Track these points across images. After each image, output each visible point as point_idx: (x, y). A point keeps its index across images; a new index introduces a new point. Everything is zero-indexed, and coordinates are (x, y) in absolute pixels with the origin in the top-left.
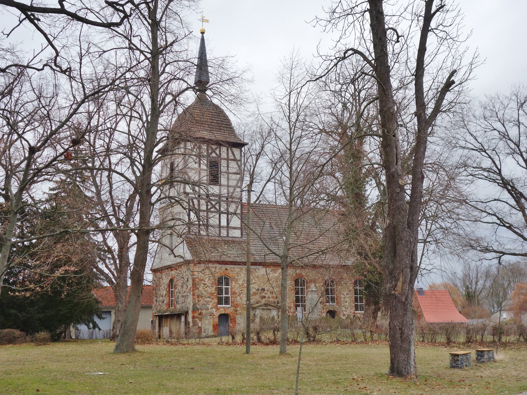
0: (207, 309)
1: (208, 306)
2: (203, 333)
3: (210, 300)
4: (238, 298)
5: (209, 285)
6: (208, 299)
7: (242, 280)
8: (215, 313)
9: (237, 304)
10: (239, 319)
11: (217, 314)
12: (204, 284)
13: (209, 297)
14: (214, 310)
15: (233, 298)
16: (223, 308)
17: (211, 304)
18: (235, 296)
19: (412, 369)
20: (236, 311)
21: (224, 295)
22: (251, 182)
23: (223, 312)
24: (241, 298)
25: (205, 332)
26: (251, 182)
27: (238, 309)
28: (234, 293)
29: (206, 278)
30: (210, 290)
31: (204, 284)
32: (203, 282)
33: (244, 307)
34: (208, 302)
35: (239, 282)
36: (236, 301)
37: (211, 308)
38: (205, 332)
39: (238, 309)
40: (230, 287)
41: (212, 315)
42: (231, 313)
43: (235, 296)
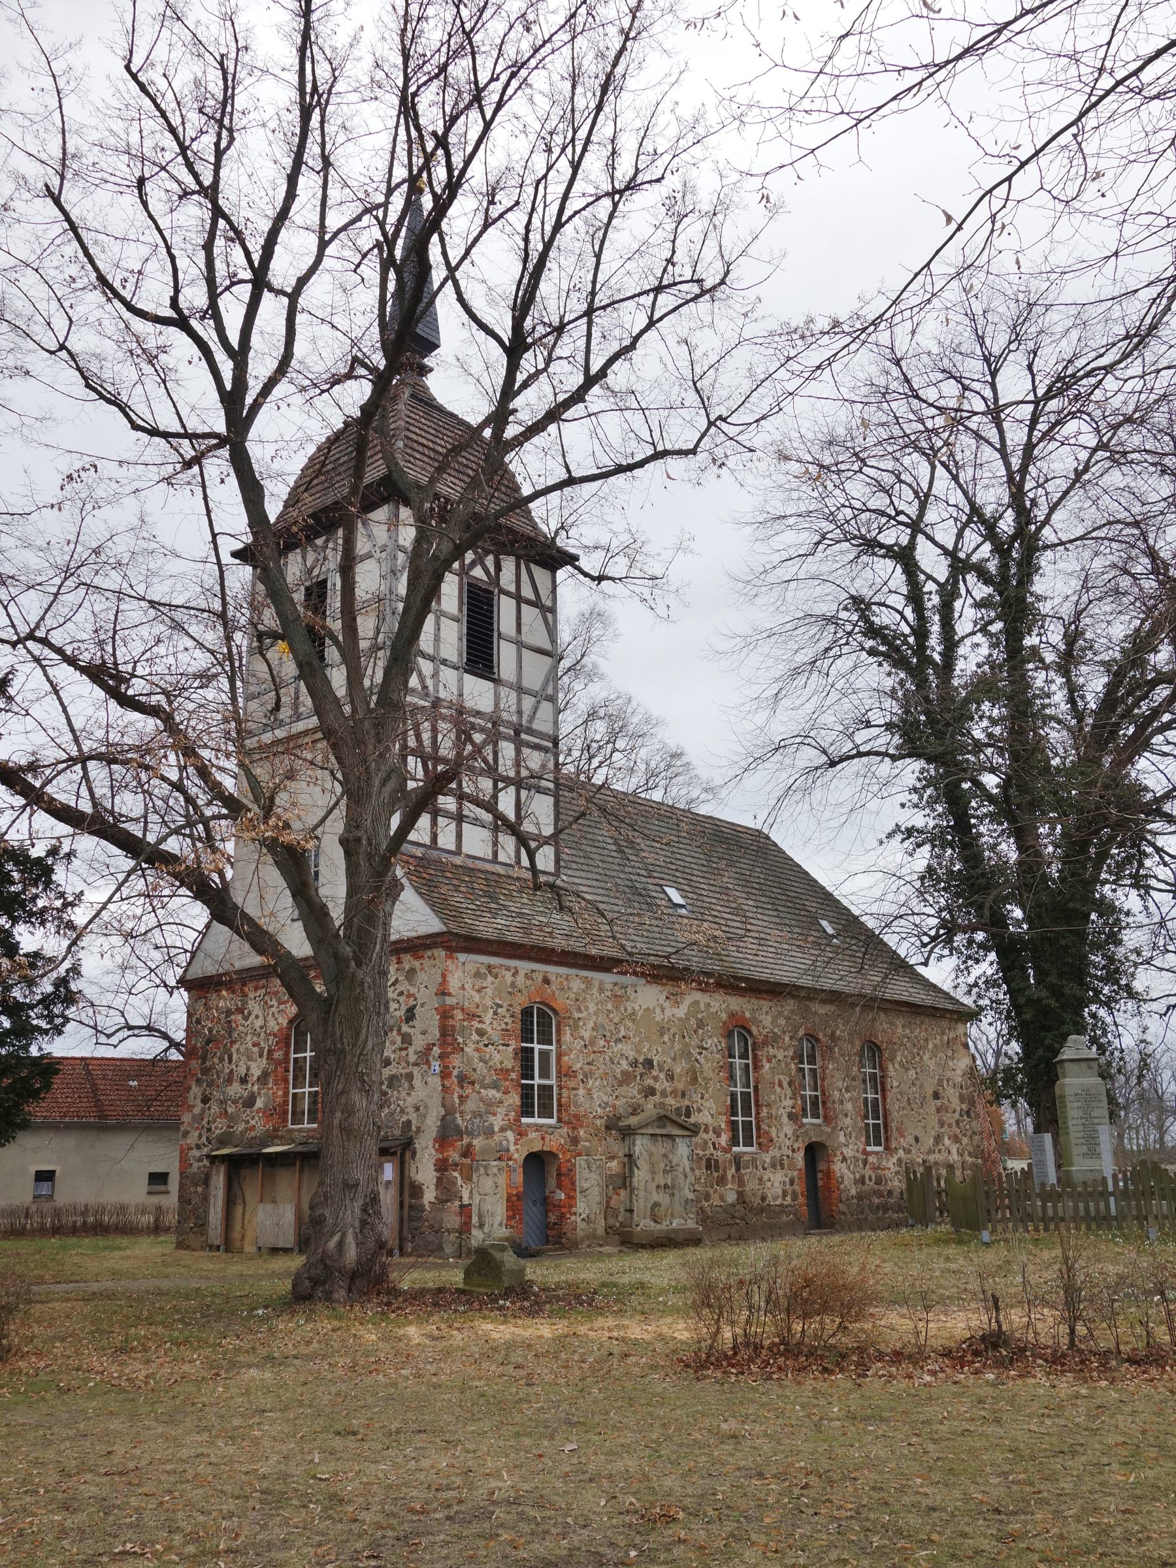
0: (489, 1132)
1: (491, 1118)
3: (498, 1095)
4: (581, 1092)
6: (492, 1093)
8: (512, 1148)
11: (519, 1154)
13: (495, 1085)
20: (575, 1140)
29: (485, 1010)
37: (502, 1130)
41: (503, 1155)
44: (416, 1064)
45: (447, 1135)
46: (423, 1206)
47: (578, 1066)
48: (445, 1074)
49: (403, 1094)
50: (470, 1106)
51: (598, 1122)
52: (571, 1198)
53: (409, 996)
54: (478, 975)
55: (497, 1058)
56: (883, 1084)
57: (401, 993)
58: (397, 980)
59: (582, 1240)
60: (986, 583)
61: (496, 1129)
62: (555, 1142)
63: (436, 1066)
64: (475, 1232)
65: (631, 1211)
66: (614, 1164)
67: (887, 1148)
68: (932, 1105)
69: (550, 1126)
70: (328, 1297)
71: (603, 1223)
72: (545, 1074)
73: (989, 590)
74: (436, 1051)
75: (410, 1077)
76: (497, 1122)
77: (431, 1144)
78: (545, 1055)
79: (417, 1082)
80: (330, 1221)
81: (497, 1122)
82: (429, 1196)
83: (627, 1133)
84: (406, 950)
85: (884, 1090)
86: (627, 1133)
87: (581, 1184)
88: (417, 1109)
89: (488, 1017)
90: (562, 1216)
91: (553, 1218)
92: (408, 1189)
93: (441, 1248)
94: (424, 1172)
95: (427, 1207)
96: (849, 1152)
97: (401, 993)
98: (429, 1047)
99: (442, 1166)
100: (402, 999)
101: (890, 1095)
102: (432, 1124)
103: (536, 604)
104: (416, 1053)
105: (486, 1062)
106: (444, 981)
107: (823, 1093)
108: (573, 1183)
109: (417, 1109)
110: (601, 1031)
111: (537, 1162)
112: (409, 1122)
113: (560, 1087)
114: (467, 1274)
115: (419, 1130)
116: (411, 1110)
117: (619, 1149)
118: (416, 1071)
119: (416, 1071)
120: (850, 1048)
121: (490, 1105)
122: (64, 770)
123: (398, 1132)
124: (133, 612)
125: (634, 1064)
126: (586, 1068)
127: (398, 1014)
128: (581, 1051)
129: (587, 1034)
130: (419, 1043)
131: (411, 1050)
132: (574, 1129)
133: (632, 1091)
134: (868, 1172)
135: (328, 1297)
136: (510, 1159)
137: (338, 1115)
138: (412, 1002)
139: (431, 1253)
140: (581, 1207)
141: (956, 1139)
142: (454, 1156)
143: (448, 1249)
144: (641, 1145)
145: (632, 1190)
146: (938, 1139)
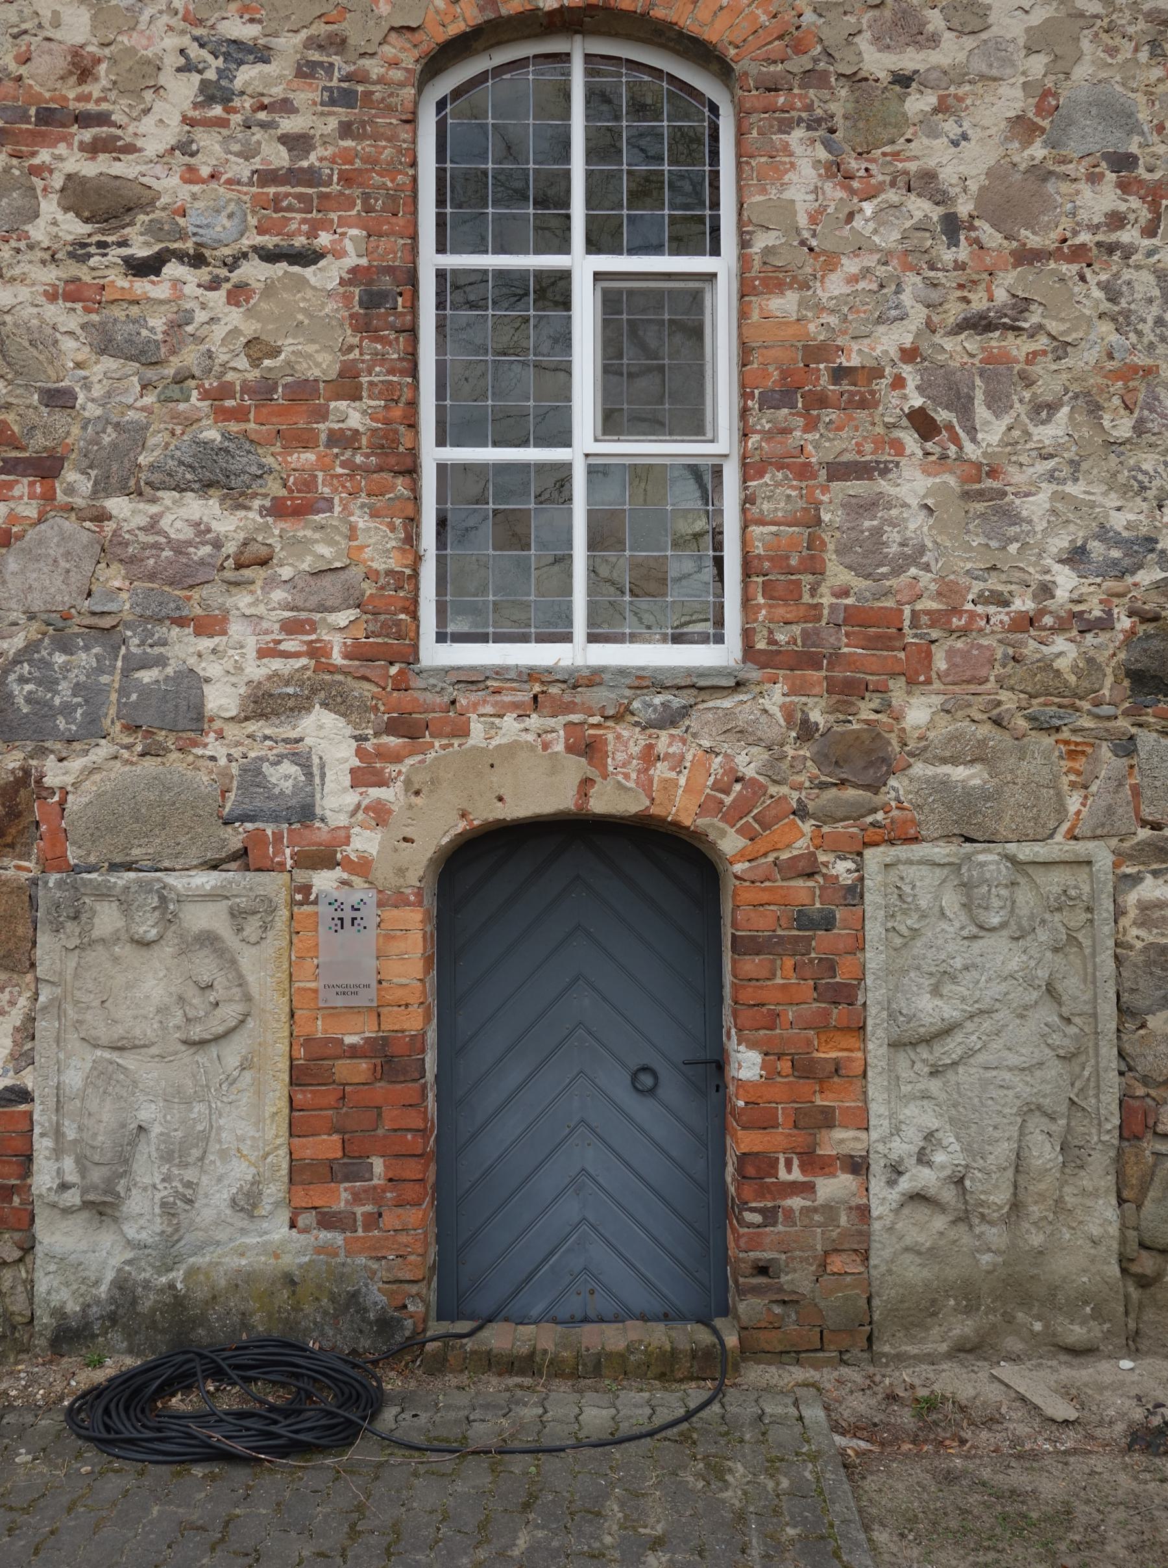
0: (177, 716)
1: (185, 648)
2: (56, 1237)
3: (230, 525)
4: (912, 483)
5: (220, 221)
6: (185, 513)
7: (1011, 99)
8: (337, 800)
9: (876, 626)
10: (945, 939)
11: (389, 830)
12: (106, 207)
13: (213, 476)
14: (328, 735)
15: (780, 495)
16: (542, 692)
17: (255, 610)
18: (820, 446)
19: (13, 831)
20: (864, 759)
21: (586, 440)
22: (1095, 969)
23: (541, 790)
24: (983, 492)
25: (102, 1209)
26: (1095, 969)
27: (918, 712)
28: (801, 384)
29: (143, 79)
30: (222, 324)
31: (106, 207)
32: (68, 159)
33: (1046, 683)
34: (181, 588)
35: (932, 153)
36: (868, 554)
37: (263, 704)
38: (102, 1209)
39: (918, 712)
40: (722, 265)
41: (268, 835)
42: (746, 803)
43: (820, 446)
47: (889, 341)
51: (1064, 651)
59: (921, 1311)
61: (221, 699)
69: (700, 686)
71: (1104, 1217)
76: (226, 669)
87: (895, 986)
89: (157, 130)
105: (144, 355)
108: (845, 994)
110: (1091, 138)
121: (186, 577)
122: (1085, 969)
124: (868, 1328)
126: (959, 350)
128: (913, 256)
129: (966, 158)
132: (846, 692)
136: (325, 859)
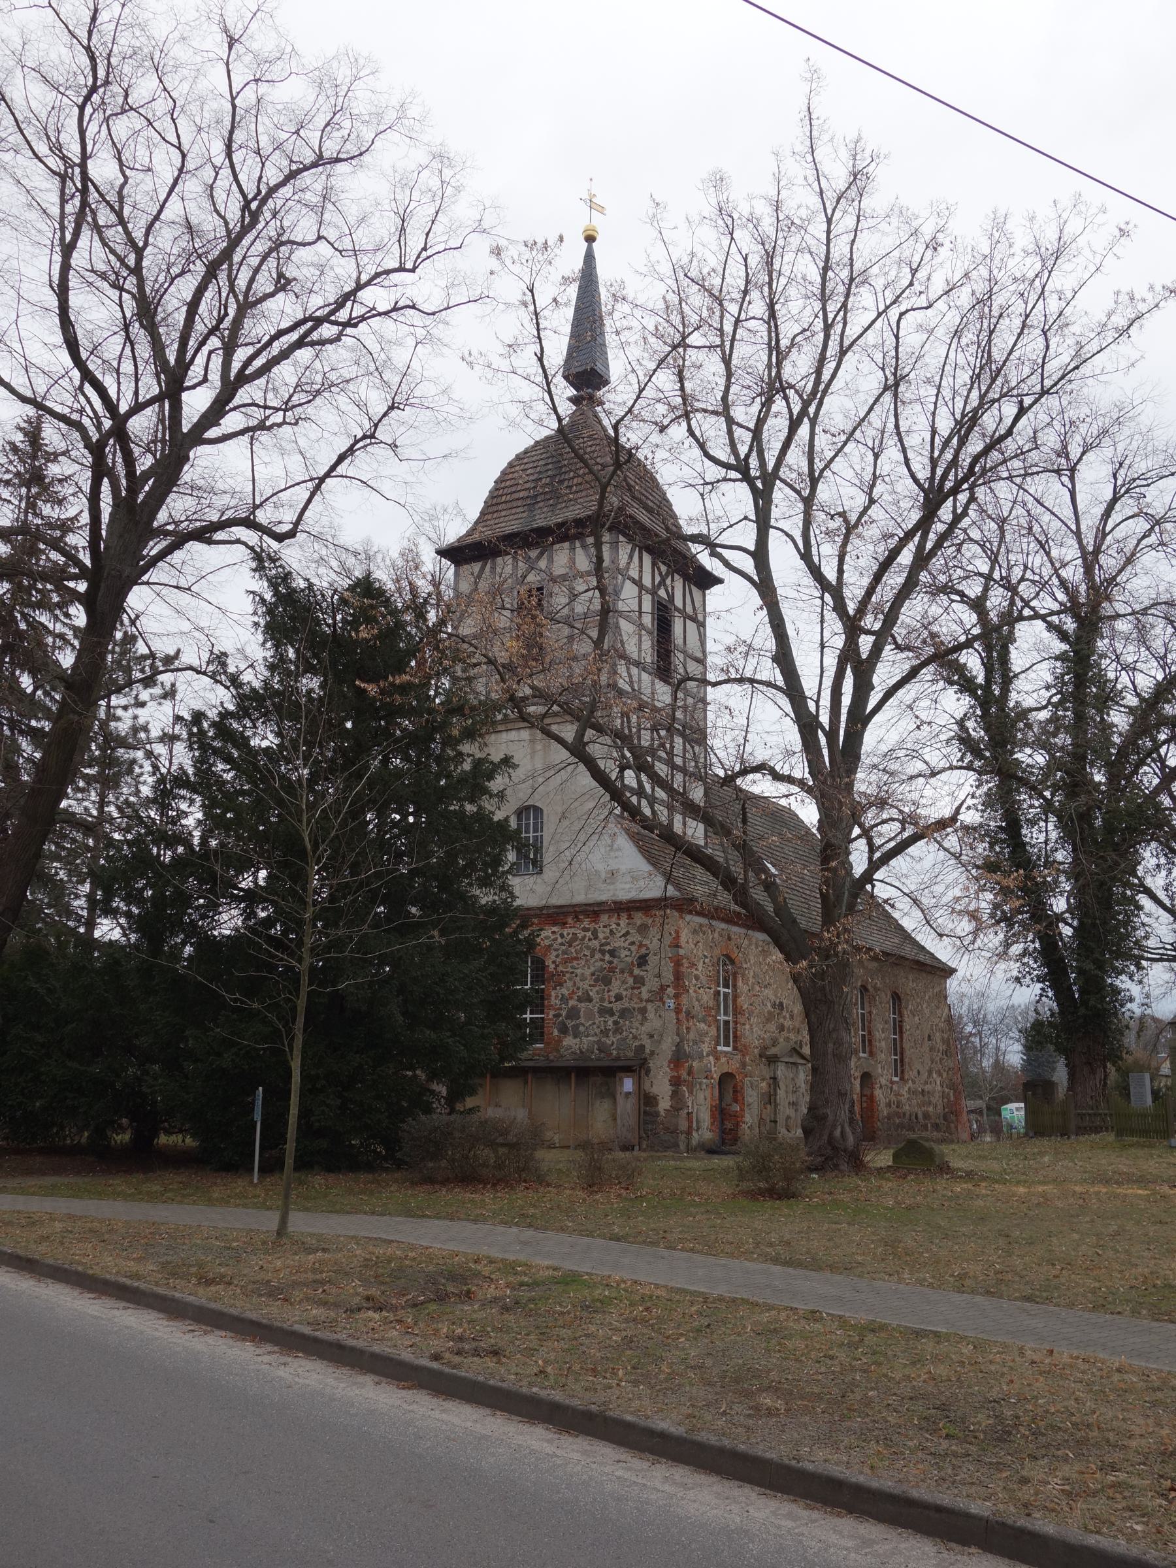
0: (701, 1057)
20: (744, 1065)
44: (648, 1001)
45: (678, 1058)
46: (657, 1114)
48: (678, 1010)
49: (636, 1024)
50: (692, 1036)
52: (742, 1110)
53: (641, 945)
54: (695, 932)
55: (705, 998)
56: (901, 1027)
57: (633, 943)
58: (627, 933)
60: (1062, 640)
62: (733, 1066)
63: (671, 1003)
64: (695, 1134)
65: (775, 1122)
66: (764, 1084)
67: (902, 1079)
68: (927, 1043)
70: (836, 1166)
72: (726, 1014)
73: (1065, 647)
74: (670, 991)
75: (643, 1011)
77: (665, 1064)
78: (726, 995)
79: (651, 1015)
80: (831, 1118)
81: (705, 1048)
82: (664, 1104)
83: (772, 1060)
84: (638, 909)
85: (901, 1032)
86: (772, 1060)
88: (652, 1036)
90: (737, 1125)
91: (729, 1125)
92: (648, 1100)
93: (676, 1145)
94: (661, 1086)
95: (662, 1113)
96: (883, 1081)
97: (633, 943)
98: (663, 989)
99: (676, 1082)
100: (633, 948)
101: (905, 1037)
102: (667, 1046)
103: (694, 619)
104: (650, 991)
106: (678, 937)
107: (870, 1033)
109: (652, 1036)
111: (726, 1078)
112: (642, 1047)
113: (736, 1023)
114: (896, 1157)
115: (652, 1053)
116: (644, 1037)
117: (766, 1072)
118: (649, 1006)
119: (649, 1006)
120: (885, 998)
123: (630, 1054)
125: (774, 1006)
127: (629, 959)
130: (652, 983)
131: (644, 989)
133: (772, 1027)
134: (893, 1098)
135: (836, 1166)
137: (831, 1045)
138: (643, 951)
139: (666, 1148)
140: (748, 1118)
141: (940, 1075)
142: (684, 1074)
143: (682, 1147)
144: (781, 1071)
145: (776, 1106)
146: (930, 1072)
